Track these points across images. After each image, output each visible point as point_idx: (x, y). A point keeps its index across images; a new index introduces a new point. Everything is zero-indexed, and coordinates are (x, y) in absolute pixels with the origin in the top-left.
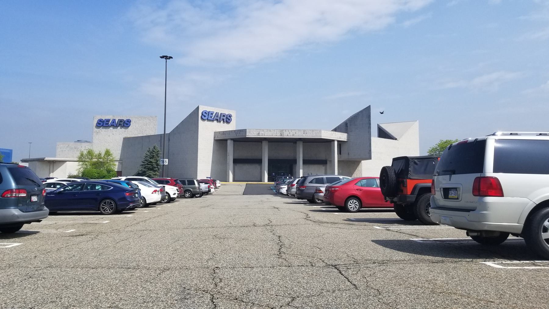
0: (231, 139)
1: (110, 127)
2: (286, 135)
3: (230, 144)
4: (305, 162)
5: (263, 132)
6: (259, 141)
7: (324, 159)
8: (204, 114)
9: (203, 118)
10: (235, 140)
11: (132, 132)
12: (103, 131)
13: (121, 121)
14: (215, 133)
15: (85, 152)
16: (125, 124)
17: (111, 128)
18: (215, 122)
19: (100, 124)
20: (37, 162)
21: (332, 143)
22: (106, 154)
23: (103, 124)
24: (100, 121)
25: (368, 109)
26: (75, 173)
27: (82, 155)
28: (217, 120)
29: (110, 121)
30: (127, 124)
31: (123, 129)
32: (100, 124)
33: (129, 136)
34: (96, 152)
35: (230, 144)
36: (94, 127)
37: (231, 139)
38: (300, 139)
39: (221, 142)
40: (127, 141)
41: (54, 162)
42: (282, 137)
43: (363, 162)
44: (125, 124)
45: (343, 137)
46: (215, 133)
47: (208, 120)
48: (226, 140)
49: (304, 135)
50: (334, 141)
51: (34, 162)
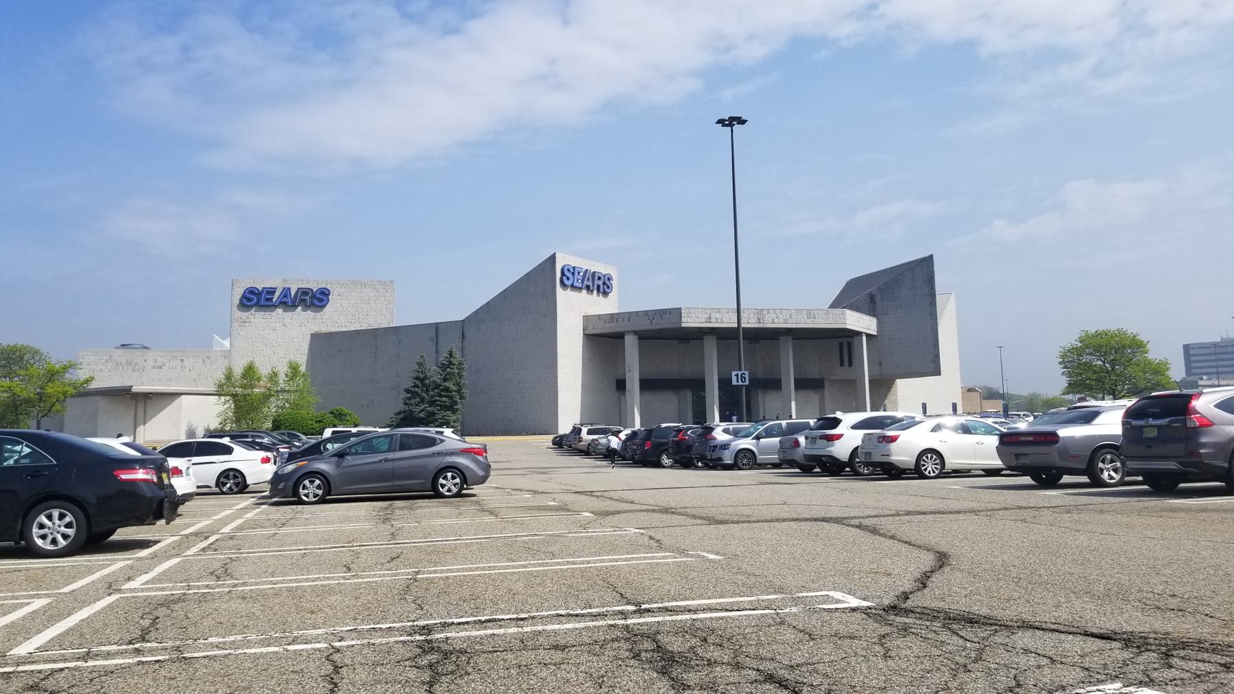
0: (635, 333)
1: (275, 306)
2: (768, 324)
3: (631, 342)
4: (647, 385)
5: (718, 315)
6: (699, 335)
7: (817, 376)
8: (566, 273)
9: (566, 282)
10: (645, 337)
11: (336, 318)
12: (258, 318)
13: (304, 292)
14: (587, 319)
15: (238, 371)
16: (315, 299)
17: (279, 311)
18: (584, 292)
19: (249, 300)
20: (99, 398)
21: (856, 339)
22: (244, 376)
23: (256, 300)
24: (252, 292)
25: (931, 256)
26: (215, 424)
27: (228, 377)
28: (588, 287)
29: (277, 294)
30: (321, 300)
31: (310, 313)
32: (249, 300)
33: (324, 329)
34: (263, 370)
35: (631, 342)
36: (235, 308)
37: (635, 333)
38: (712, 331)
39: (604, 342)
40: (321, 343)
41: (147, 396)
42: (761, 326)
43: (900, 383)
44: (315, 299)
45: (862, 323)
46: (587, 319)
47: (573, 287)
48: (620, 336)
49: (809, 321)
50: (859, 334)
51: (89, 399)
